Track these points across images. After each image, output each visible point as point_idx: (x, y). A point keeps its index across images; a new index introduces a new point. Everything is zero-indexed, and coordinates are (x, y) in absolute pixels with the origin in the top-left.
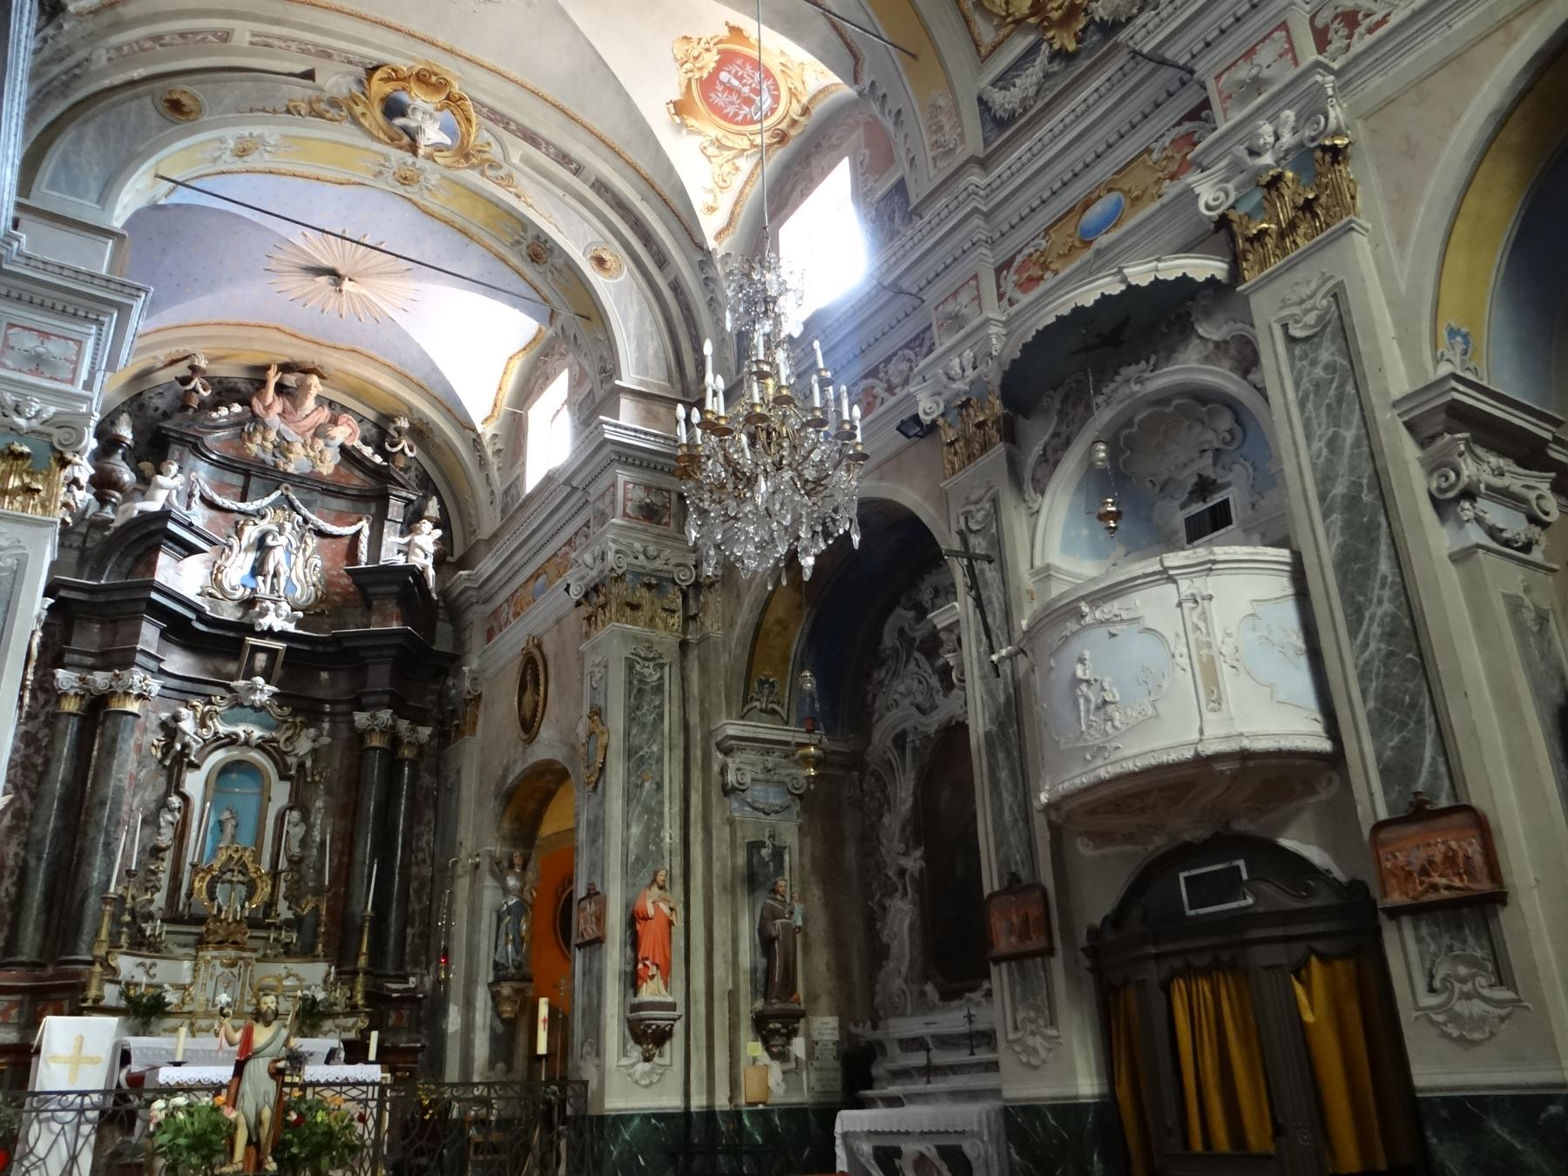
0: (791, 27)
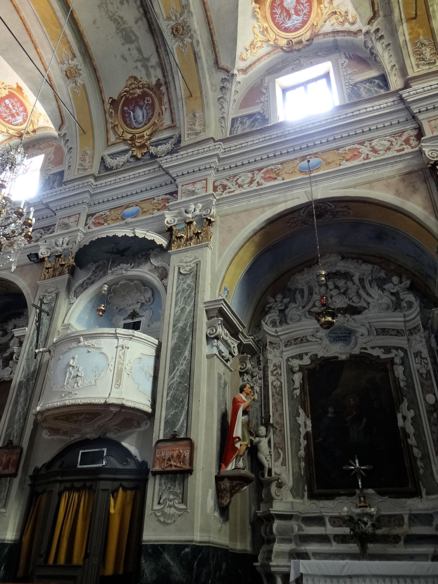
0: (43, 99)
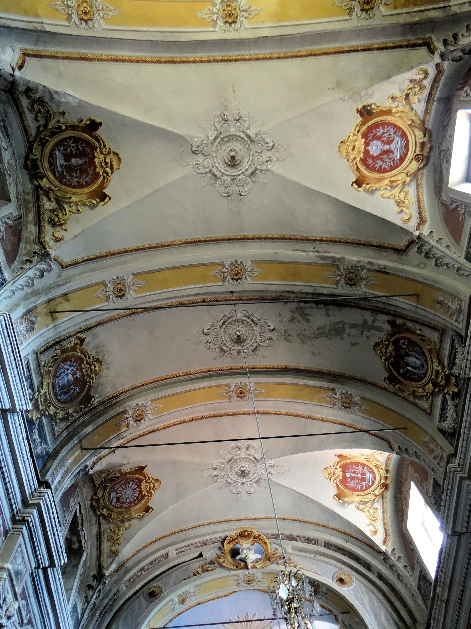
0: (358, 444)
